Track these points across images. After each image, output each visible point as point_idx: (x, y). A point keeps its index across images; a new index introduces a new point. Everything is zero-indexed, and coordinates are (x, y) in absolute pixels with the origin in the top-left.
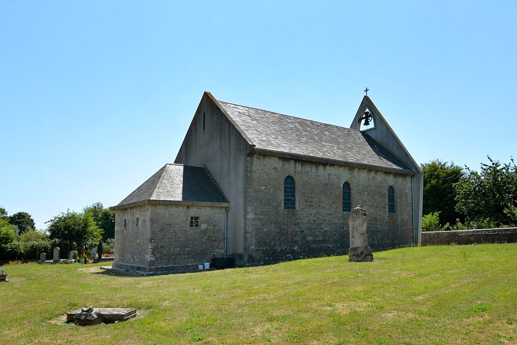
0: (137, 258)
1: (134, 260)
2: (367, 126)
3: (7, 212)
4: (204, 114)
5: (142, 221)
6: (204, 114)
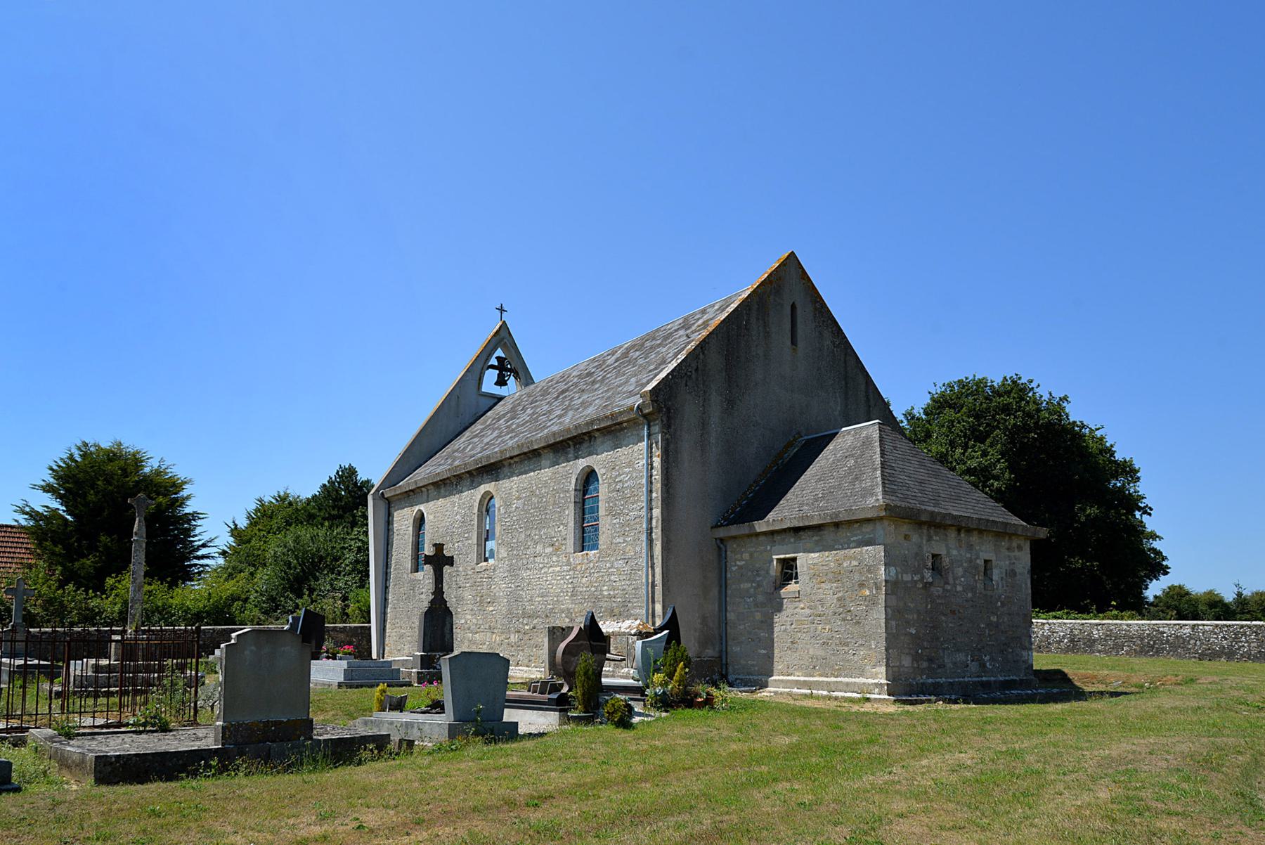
0: (992, 659)
1: (983, 665)
2: (502, 387)
3: (1112, 446)
4: (793, 307)
5: (1004, 571)
6: (793, 307)
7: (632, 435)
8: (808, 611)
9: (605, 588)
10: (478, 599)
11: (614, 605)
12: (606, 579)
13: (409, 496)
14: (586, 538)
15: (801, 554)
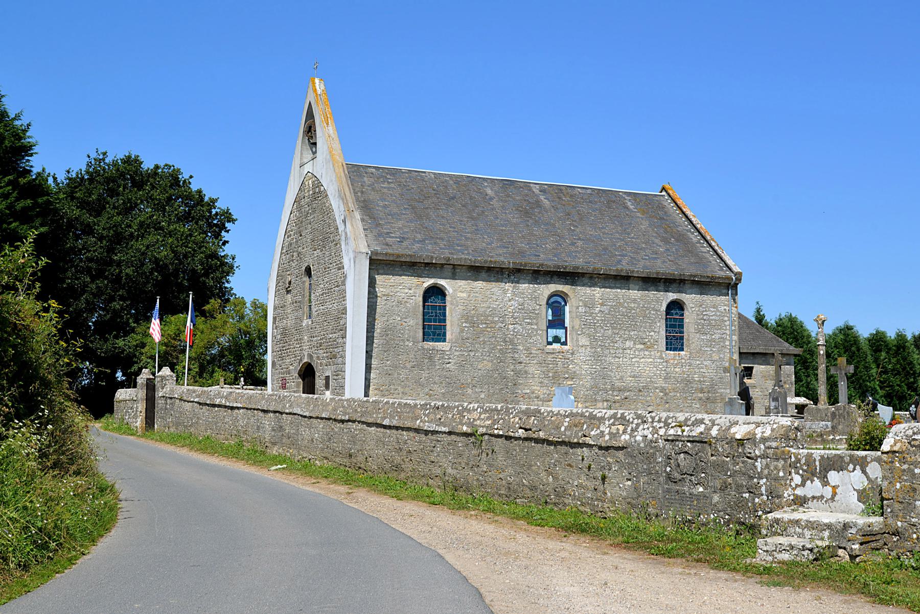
7: (715, 290)
8: (760, 393)
9: (696, 376)
10: (551, 375)
11: (704, 386)
12: (697, 371)
13: (402, 265)
14: (675, 342)
15: (756, 365)
